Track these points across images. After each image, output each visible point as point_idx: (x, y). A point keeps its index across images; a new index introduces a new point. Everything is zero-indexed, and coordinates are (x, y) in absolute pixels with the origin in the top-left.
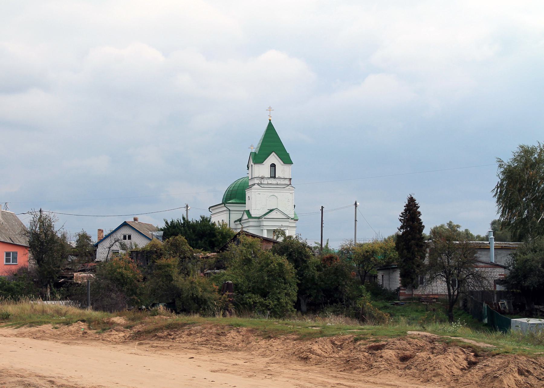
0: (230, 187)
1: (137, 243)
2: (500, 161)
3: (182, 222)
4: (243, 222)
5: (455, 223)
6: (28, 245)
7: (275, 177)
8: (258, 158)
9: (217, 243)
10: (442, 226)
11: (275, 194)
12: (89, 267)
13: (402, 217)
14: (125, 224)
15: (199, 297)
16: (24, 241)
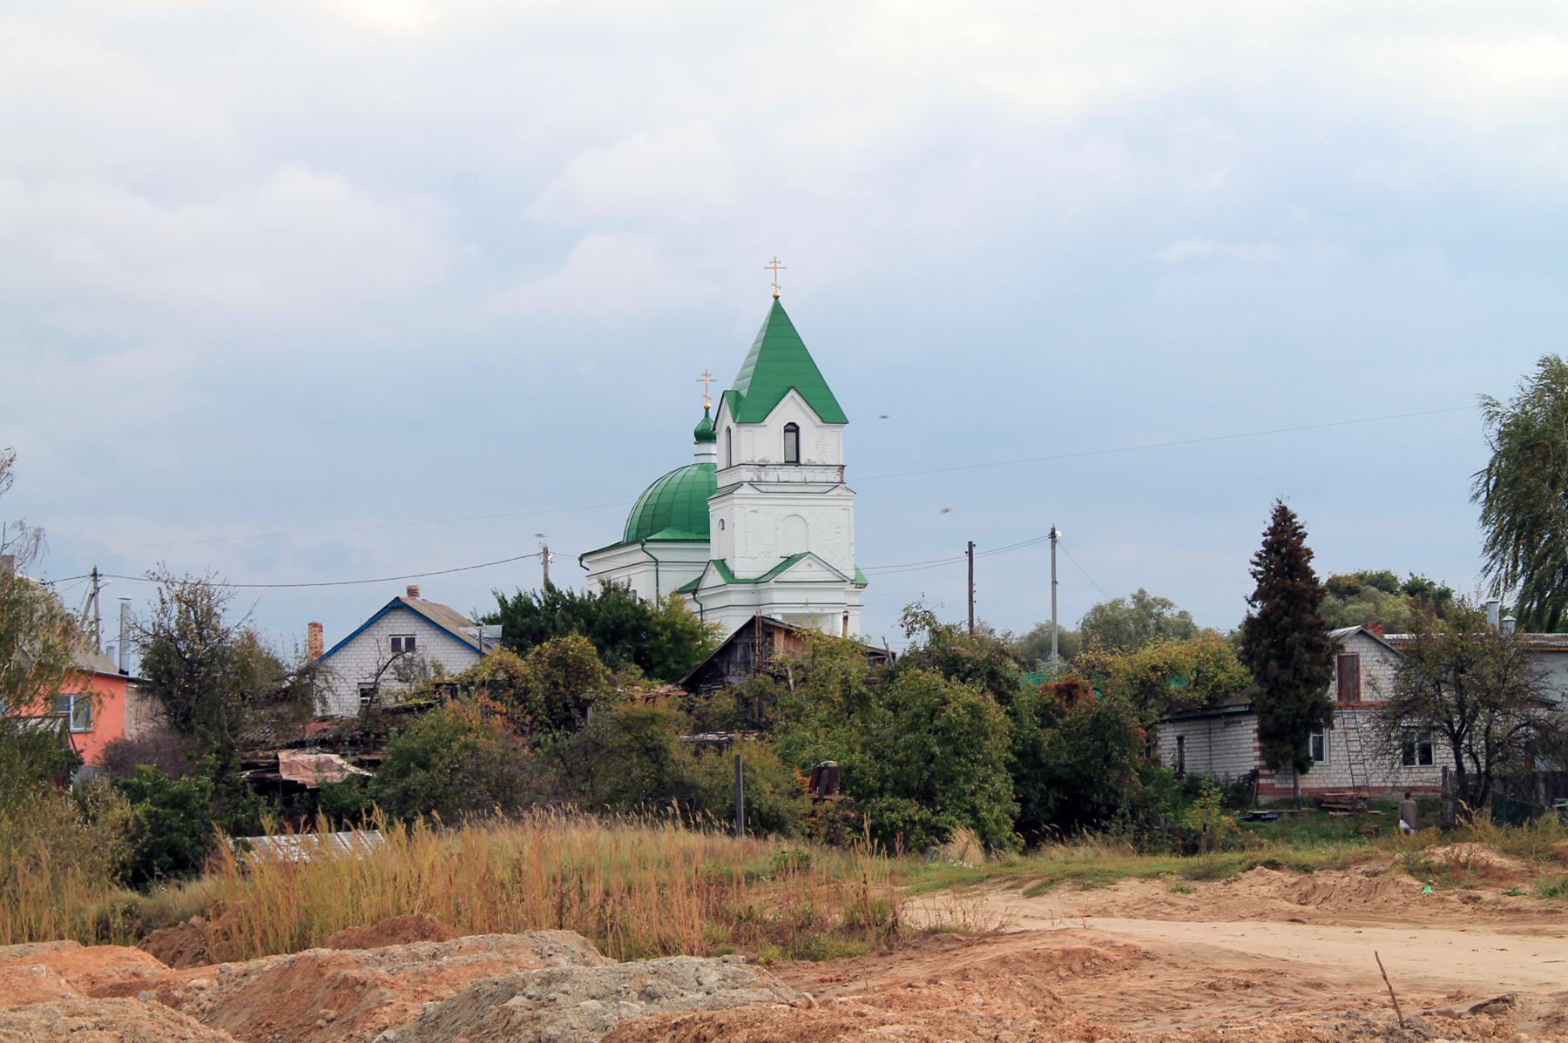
1: (442, 660)
2: (1490, 403)
4: (701, 594)
5: (1153, 593)
7: (797, 462)
8: (749, 405)
10: (1115, 605)
11: (801, 511)
13: (1257, 564)
14: (397, 606)
15: (765, 809)
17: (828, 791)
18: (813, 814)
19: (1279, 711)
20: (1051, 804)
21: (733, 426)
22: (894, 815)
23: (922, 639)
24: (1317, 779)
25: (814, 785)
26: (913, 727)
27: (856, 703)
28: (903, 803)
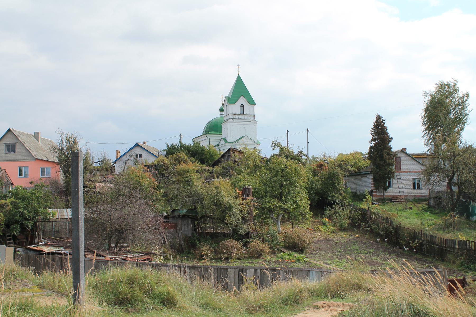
0: (208, 124)
3: (179, 145)
4: (220, 146)
6: (57, 160)
7: (243, 114)
8: (231, 100)
9: (206, 160)
11: (244, 126)
12: (108, 180)
14: (137, 145)
16: (53, 157)
17: (248, 196)
18: (243, 204)
19: (380, 173)
20: (316, 199)
21: (227, 105)
22: (270, 204)
23: (277, 151)
24: (389, 193)
25: (243, 194)
26: (276, 175)
27: (257, 168)
28: (273, 200)
